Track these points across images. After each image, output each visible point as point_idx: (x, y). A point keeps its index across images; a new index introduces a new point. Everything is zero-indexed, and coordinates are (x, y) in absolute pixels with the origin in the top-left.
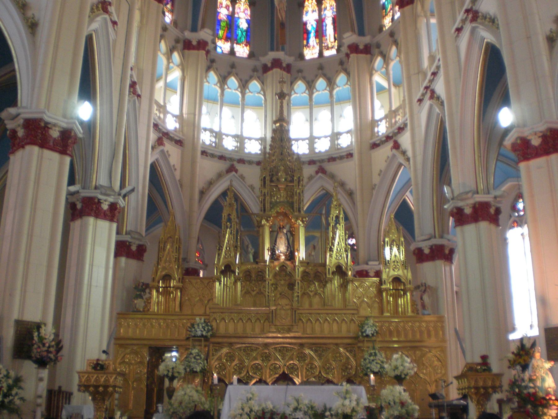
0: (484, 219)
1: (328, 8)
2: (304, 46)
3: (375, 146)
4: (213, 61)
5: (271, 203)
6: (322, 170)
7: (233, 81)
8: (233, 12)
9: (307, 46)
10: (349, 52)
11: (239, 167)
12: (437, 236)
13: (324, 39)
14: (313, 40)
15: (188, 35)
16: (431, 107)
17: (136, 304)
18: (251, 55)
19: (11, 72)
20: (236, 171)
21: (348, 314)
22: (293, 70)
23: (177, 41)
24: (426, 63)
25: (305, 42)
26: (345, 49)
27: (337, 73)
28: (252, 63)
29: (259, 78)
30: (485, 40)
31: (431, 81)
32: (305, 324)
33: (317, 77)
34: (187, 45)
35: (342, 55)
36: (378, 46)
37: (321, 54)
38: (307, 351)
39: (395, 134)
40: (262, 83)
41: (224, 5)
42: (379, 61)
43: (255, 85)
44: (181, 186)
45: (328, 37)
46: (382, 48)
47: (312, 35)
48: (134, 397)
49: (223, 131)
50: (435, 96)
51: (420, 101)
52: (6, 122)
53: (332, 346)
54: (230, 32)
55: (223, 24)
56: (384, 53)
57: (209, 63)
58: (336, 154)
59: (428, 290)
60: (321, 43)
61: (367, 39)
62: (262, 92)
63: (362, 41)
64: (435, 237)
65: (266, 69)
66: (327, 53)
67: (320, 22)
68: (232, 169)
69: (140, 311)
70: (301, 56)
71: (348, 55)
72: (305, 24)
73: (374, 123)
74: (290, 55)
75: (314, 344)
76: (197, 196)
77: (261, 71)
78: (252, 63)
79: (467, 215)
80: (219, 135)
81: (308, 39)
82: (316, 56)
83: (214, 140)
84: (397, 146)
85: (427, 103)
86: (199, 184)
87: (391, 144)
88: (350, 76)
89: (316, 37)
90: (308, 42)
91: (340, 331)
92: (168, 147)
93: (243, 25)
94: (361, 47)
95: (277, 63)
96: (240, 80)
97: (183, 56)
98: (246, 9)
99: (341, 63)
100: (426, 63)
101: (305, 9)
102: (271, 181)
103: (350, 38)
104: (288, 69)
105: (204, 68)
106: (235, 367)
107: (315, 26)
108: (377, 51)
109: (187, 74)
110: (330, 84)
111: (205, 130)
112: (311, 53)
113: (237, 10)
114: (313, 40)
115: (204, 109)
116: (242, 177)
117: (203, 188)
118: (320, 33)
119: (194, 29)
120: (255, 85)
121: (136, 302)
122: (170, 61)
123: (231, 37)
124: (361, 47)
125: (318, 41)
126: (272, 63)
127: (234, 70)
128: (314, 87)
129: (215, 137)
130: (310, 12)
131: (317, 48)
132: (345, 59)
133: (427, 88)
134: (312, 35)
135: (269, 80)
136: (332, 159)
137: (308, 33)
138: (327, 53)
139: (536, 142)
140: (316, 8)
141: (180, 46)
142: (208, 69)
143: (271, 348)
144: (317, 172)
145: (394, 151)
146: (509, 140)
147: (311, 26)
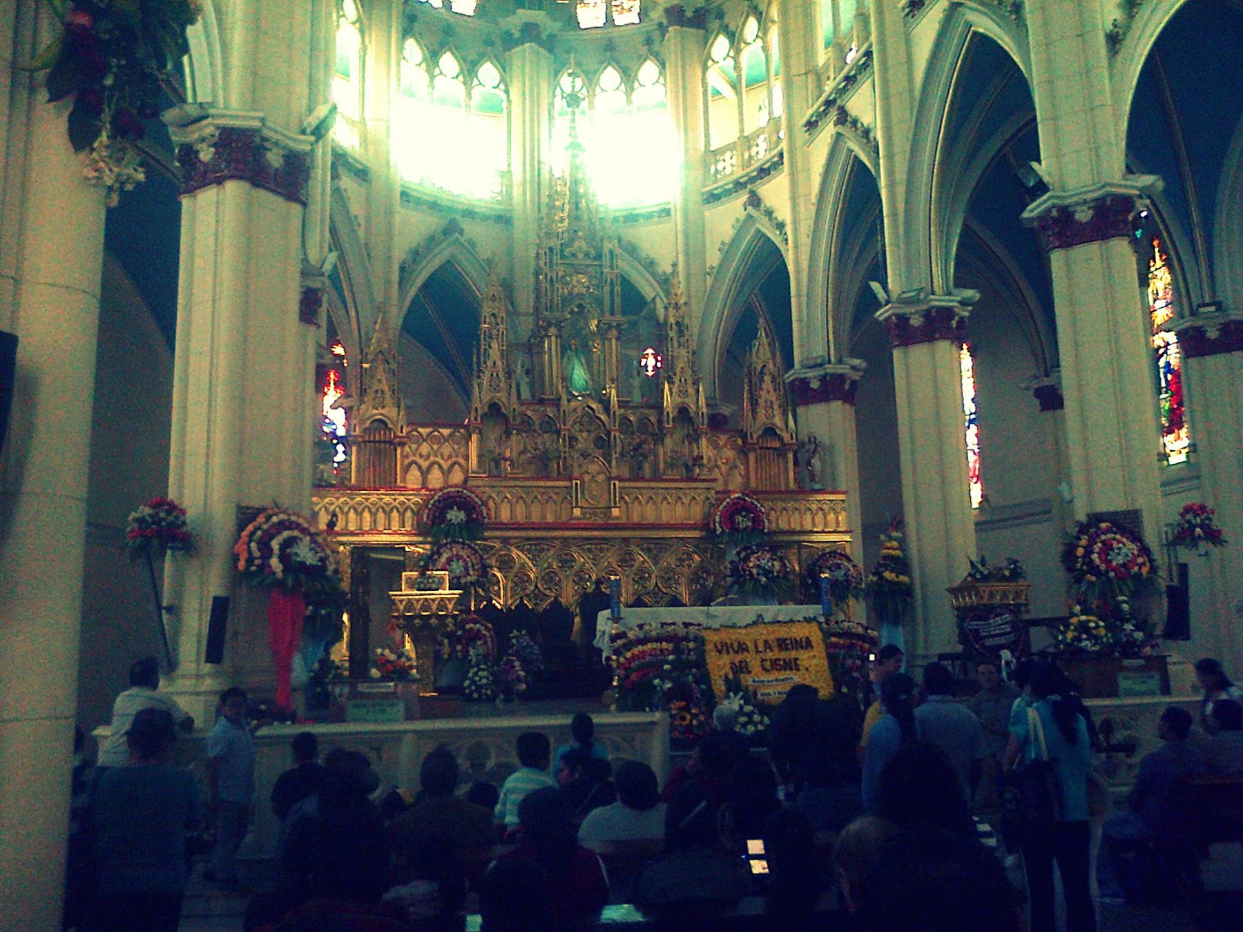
0: (943, 338)
7: (448, 62)
10: (665, 21)
12: (832, 359)
16: (839, 136)
17: (322, 472)
19: (1027, 124)
21: (643, 488)
24: (822, 56)
26: (657, 15)
27: (642, 60)
29: (496, 57)
30: (972, 29)
31: (841, 92)
32: (630, 506)
35: (648, 26)
37: (609, 20)
38: (515, 553)
39: (752, 180)
40: (504, 67)
42: (721, 45)
48: (342, 634)
50: (849, 119)
51: (811, 125)
52: (171, 129)
53: (675, 540)
56: (732, 27)
58: (415, 190)
59: (819, 449)
62: (502, 86)
64: (829, 362)
65: (509, 42)
66: (620, 19)
69: (333, 486)
71: (662, 28)
75: (587, 539)
76: (395, 277)
79: (916, 329)
82: (600, 22)
84: (755, 201)
85: (828, 130)
88: (664, 67)
91: (529, 516)
95: (530, 32)
96: (462, 59)
99: (649, 42)
100: (822, 56)
104: (550, 44)
106: (515, 579)
108: (715, 24)
109: (370, 42)
110: (628, 81)
117: (404, 262)
121: (322, 467)
122: (341, 13)
126: (522, 31)
127: (450, 39)
128: (597, 83)
132: (656, 35)
133: (829, 103)
135: (517, 63)
139: (1083, 215)
145: (750, 208)
146: (1032, 211)
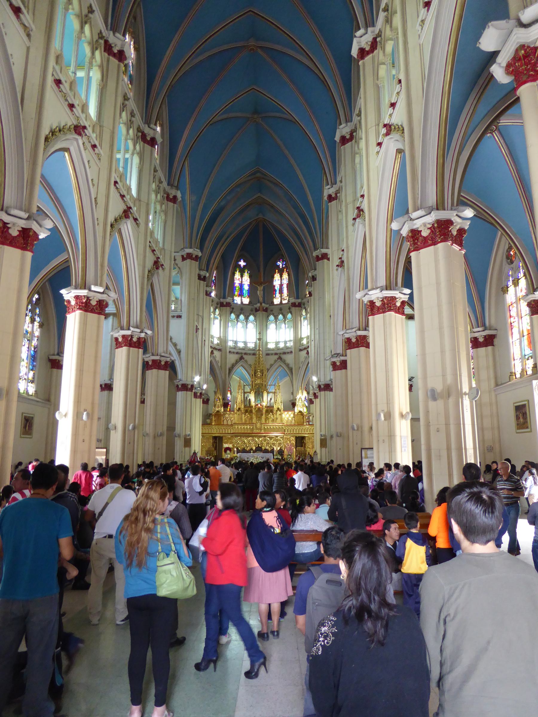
1: (285, 279)
2: (274, 298)
3: (301, 350)
4: (233, 309)
5: (255, 384)
6: (280, 358)
8: (242, 282)
9: (275, 297)
11: (245, 356)
13: (283, 294)
14: (278, 295)
15: (222, 300)
18: (250, 302)
20: (244, 359)
22: (269, 311)
23: (217, 304)
25: (274, 296)
28: (250, 307)
33: (279, 314)
34: (222, 305)
36: (304, 304)
40: (255, 316)
41: (237, 279)
43: (252, 318)
44: (221, 368)
45: (284, 294)
46: (306, 306)
47: (278, 292)
49: (238, 340)
54: (241, 292)
55: (237, 288)
57: (231, 310)
60: (281, 296)
61: (299, 301)
63: (298, 301)
65: (257, 310)
67: (281, 285)
68: (241, 358)
70: (273, 302)
72: (274, 286)
73: (302, 339)
74: (267, 304)
77: (254, 311)
78: (250, 307)
80: (236, 342)
81: (275, 294)
83: (234, 345)
86: (229, 366)
87: (305, 351)
89: (279, 293)
90: (276, 296)
92: (216, 353)
93: (246, 287)
94: (297, 304)
96: (245, 316)
97: (220, 310)
98: (248, 279)
101: (275, 278)
102: (255, 375)
103: (293, 300)
105: (229, 312)
107: (279, 288)
111: (230, 341)
112: (277, 301)
113: (243, 280)
114: (278, 295)
115: (230, 324)
116: (246, 361)
118: (281, 292)
119: (224, 298)
120: (252, 318)
123: (241, 295)
124: (297, 304)
125: (280, 295)
128: (278, 319)
129: (235, 343)
130: (277, 280)
131: (280, 298)
134: (278, 292)
135: (258, 316)
136: (284, 353)
137: (275, 290)
138: (284, 302)
140: (280, 279)
141: (219, 306)
142: (231, 313)
143: (279, 438)
144: (278, 359)
147: (277, 288)
